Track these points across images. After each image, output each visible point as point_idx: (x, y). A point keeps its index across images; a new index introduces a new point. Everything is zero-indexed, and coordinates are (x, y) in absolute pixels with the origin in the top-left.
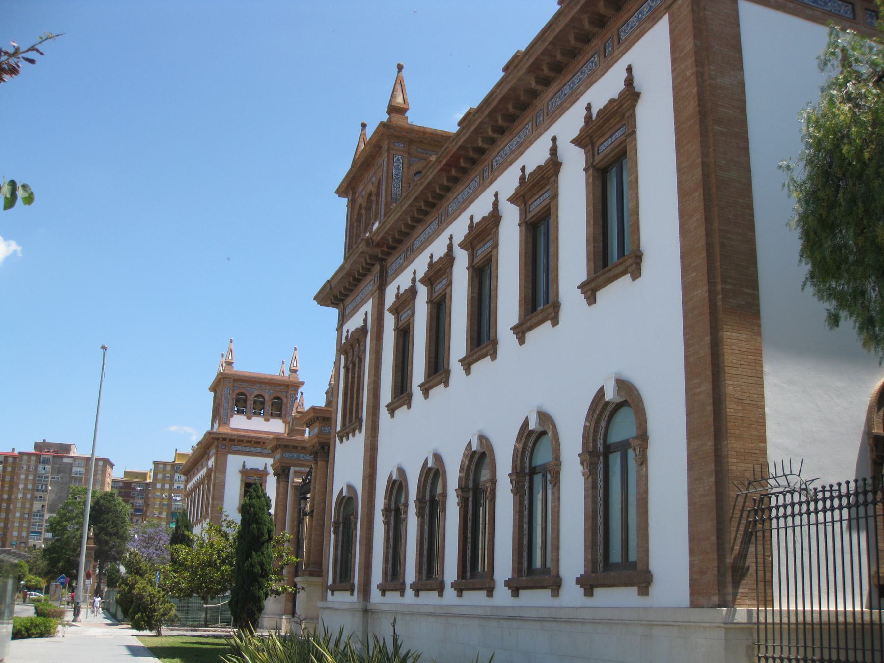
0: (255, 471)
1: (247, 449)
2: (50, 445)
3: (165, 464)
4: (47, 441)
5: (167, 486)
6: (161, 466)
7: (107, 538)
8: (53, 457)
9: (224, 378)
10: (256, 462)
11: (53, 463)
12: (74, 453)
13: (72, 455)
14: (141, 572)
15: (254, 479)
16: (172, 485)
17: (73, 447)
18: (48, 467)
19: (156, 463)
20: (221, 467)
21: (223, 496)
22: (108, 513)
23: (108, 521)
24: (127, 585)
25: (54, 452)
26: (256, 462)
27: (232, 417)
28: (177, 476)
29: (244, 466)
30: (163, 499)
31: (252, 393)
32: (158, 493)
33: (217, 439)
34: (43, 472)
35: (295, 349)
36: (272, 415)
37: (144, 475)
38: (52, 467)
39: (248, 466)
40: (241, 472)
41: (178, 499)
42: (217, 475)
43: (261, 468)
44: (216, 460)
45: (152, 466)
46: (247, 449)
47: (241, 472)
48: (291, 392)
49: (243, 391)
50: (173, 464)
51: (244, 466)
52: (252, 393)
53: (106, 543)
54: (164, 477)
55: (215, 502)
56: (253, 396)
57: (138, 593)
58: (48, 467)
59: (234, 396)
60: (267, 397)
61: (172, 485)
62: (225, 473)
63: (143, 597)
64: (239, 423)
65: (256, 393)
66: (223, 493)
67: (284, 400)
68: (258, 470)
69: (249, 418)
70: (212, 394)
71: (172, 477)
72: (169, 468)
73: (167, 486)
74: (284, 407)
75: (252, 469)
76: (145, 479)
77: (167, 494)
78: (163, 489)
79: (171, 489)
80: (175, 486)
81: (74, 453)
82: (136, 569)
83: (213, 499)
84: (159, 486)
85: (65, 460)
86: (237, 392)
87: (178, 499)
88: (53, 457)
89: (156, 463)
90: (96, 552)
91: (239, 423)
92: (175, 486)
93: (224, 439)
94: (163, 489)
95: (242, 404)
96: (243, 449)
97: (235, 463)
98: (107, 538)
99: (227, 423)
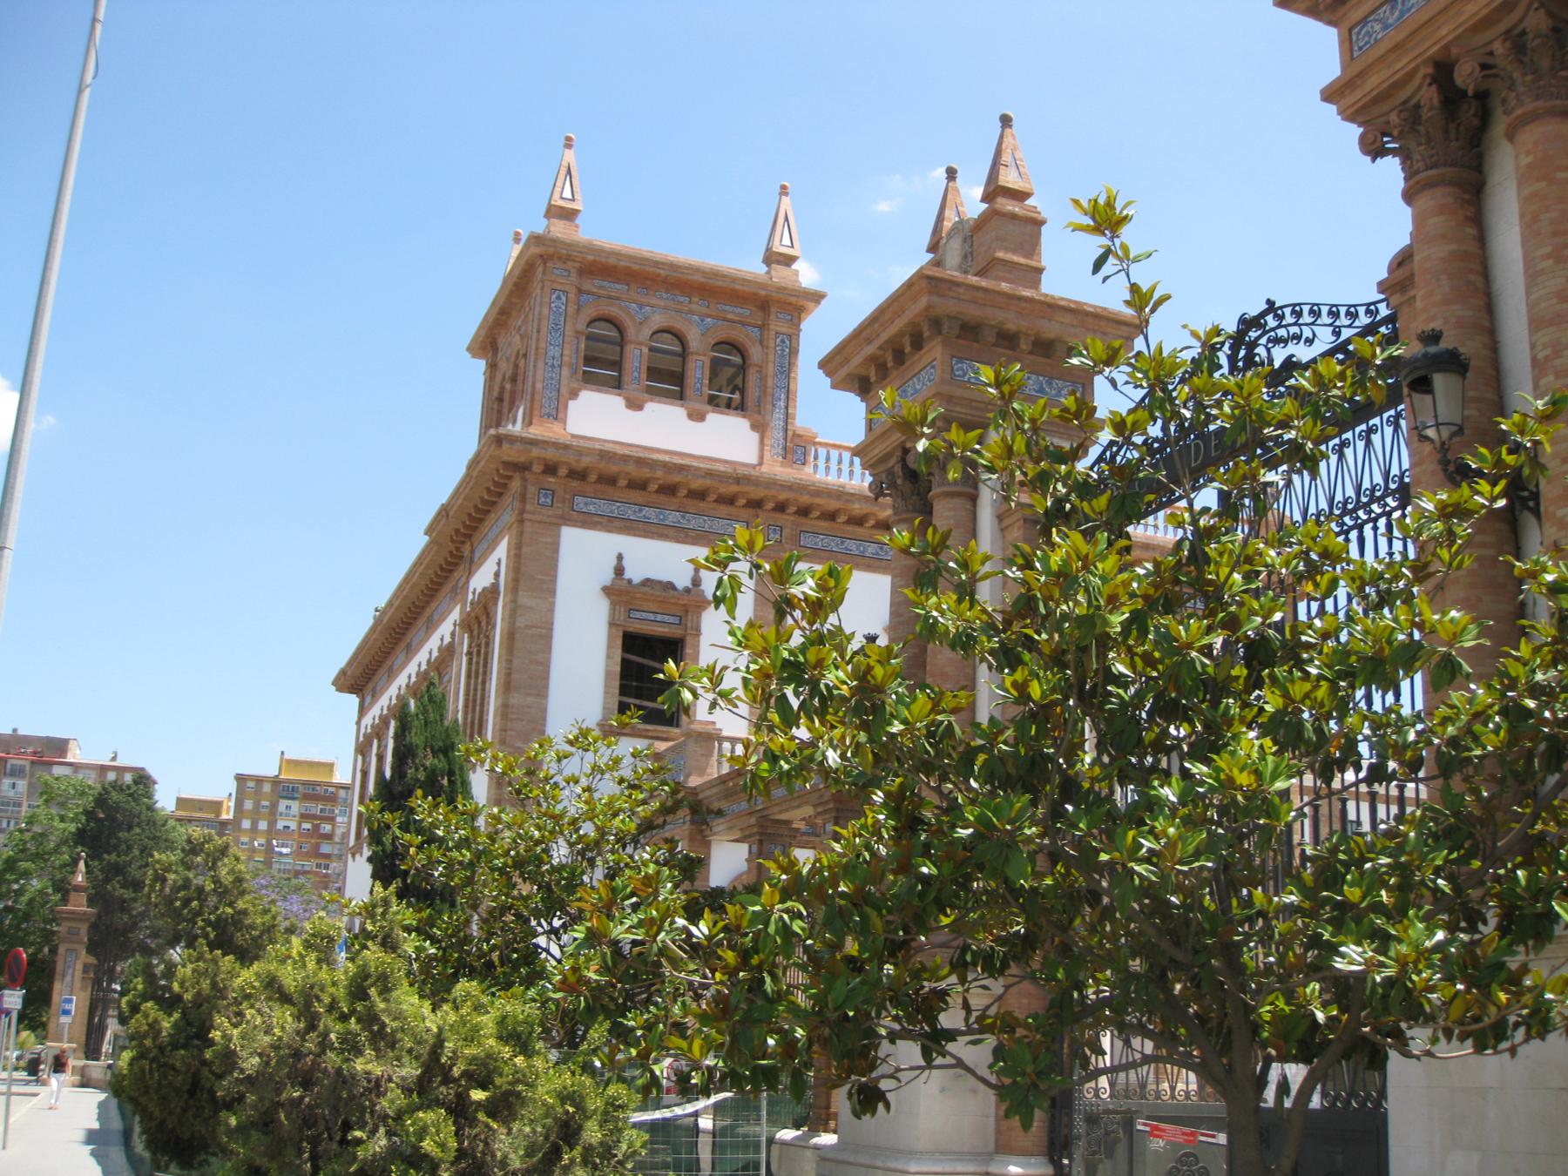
0: (660, 590)
1: (630, 512)
2: (28, 740)
3: (259, 780)
4: (21, 732)
5: (263, 825)
6: (251, 784)
7: (128, 894)
8: (33, 763)
9: (545, 259)
10: (664, 560)
11: (32, 775)
12: (75, 755)
13: (70, 759)
14: (240, 938)
15: (657, 625)
16: (272, 823)
17: (72, 745)
18: (22, 785)
19: (241, 779)
20: (535, 575)
21: (545, 678)
22: (130, 828)
23: (129, 848)
24: (170, 1003)
25: (35, 753)
26: (664, 560)
27: (574, 394)
28: (283, 804)
29: (619, 571)
30: (254, 850)
31: (647, 317)
32: (244, 839)
33: (522, 468)
34: (11, 793)
35: (784, 190)
36: (713, 401)
37: (216, 806)
38: (30, 785)
39: (635, 573)
40: (607, 591)
41: (285, 850)
42: (524, 598)
43: (682, 580)
44: (517, 555)
45: (232, 787)
46: (630, 512)
47: (607, 591)
48: (778, 325)
49: (612, 310)
50: (275, 781)
51: (619, 571)
52: (647, 317)
53: (124, 906)
54: (257, 806)
55: (515, 699)
56: (647, 332)
57: (295, 1065)
58: (22, 785)
59: (581, 326)
60: (694, 342)
61: (272, 823)
62: (553, 592)
63: (349, 1104)
64: (599, 419)
65: (658, 320)
66: (546, 665)
67: (755, 353)
68: (670, 586)
69: (635, 405)
70: (481, 365)
71: (274, 806)
72: (267, 788)
73: (263, 825)
74: (753, 378)
75: (647, 582)
76: (218, 814)
77: (262, 841)
78: (254, 829)
79: (271, 832)
80: (280, 825)
81: (75, 755)
82: (219, 924)
83: (507, 686)
84: (246, 824)
85: (58, 771)
86: (590, 312)
87: (285, 850)
88: (33, 763)
89: (241, 779)
90: (94, 927)
91: (599, 419)
92: (280, 825)
93: (551, 469)
94: (254, 829)
95: (603, 365)
96: (615, 509)
97: (587, 558)
98: (128, 894)
99: (558, 414)
